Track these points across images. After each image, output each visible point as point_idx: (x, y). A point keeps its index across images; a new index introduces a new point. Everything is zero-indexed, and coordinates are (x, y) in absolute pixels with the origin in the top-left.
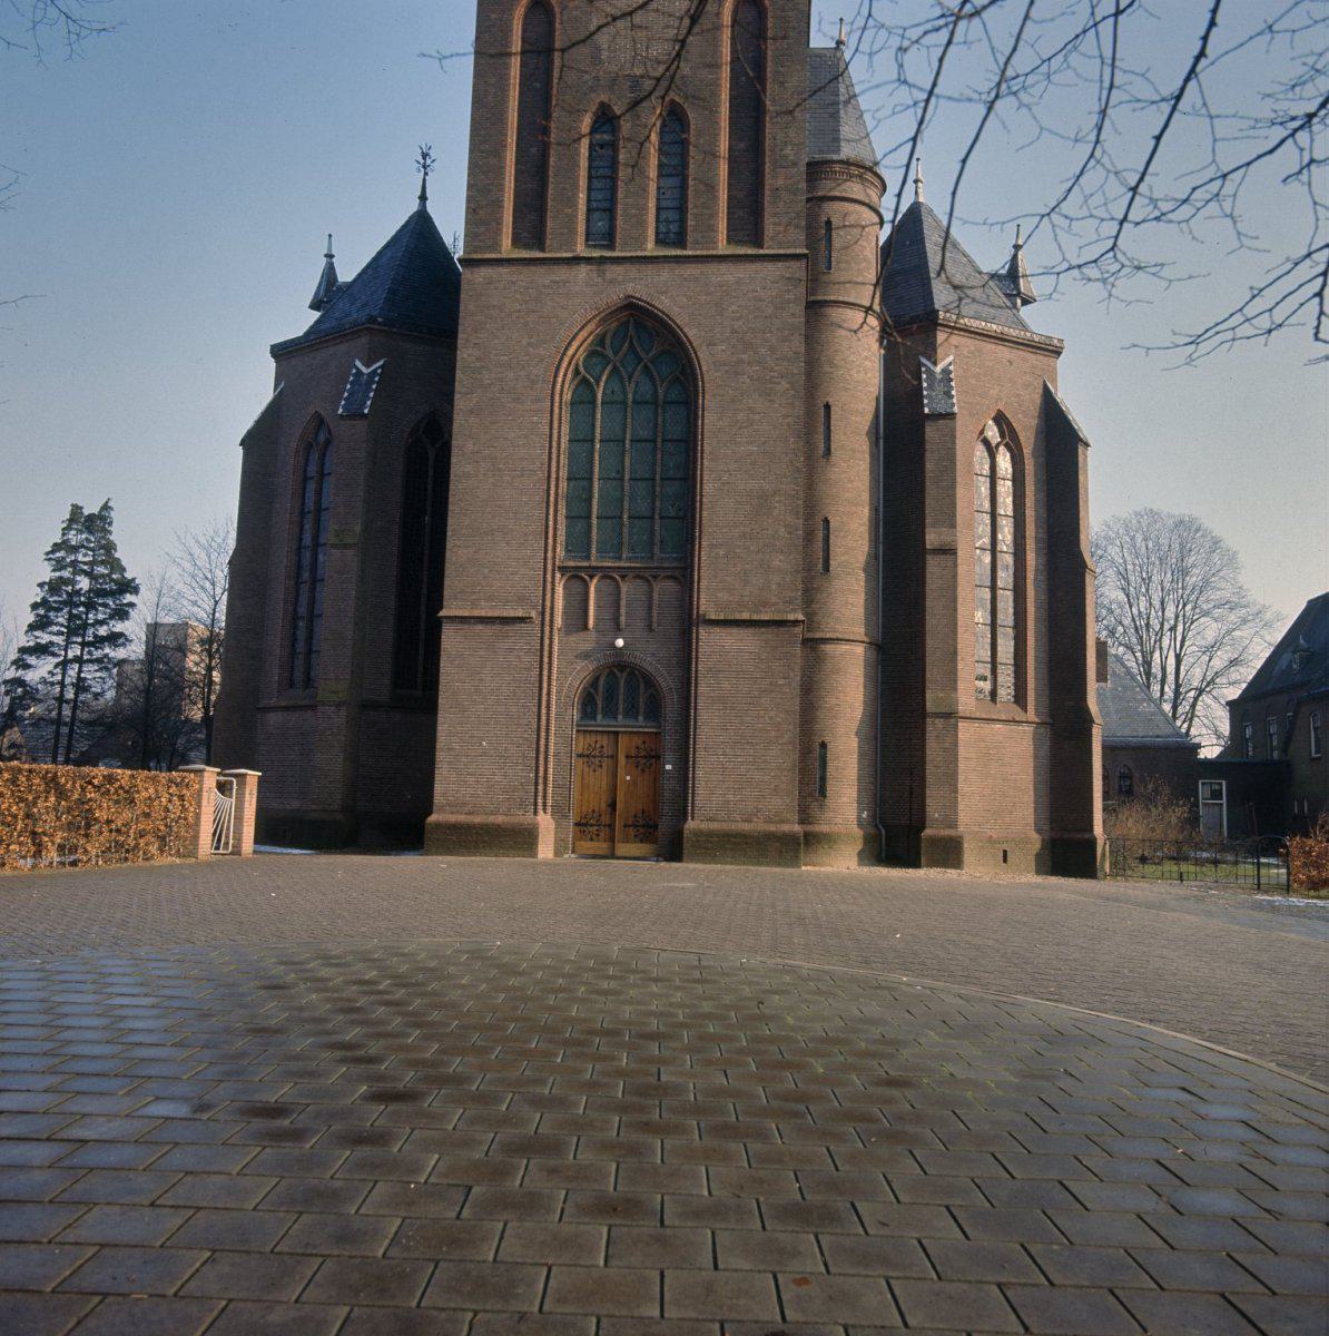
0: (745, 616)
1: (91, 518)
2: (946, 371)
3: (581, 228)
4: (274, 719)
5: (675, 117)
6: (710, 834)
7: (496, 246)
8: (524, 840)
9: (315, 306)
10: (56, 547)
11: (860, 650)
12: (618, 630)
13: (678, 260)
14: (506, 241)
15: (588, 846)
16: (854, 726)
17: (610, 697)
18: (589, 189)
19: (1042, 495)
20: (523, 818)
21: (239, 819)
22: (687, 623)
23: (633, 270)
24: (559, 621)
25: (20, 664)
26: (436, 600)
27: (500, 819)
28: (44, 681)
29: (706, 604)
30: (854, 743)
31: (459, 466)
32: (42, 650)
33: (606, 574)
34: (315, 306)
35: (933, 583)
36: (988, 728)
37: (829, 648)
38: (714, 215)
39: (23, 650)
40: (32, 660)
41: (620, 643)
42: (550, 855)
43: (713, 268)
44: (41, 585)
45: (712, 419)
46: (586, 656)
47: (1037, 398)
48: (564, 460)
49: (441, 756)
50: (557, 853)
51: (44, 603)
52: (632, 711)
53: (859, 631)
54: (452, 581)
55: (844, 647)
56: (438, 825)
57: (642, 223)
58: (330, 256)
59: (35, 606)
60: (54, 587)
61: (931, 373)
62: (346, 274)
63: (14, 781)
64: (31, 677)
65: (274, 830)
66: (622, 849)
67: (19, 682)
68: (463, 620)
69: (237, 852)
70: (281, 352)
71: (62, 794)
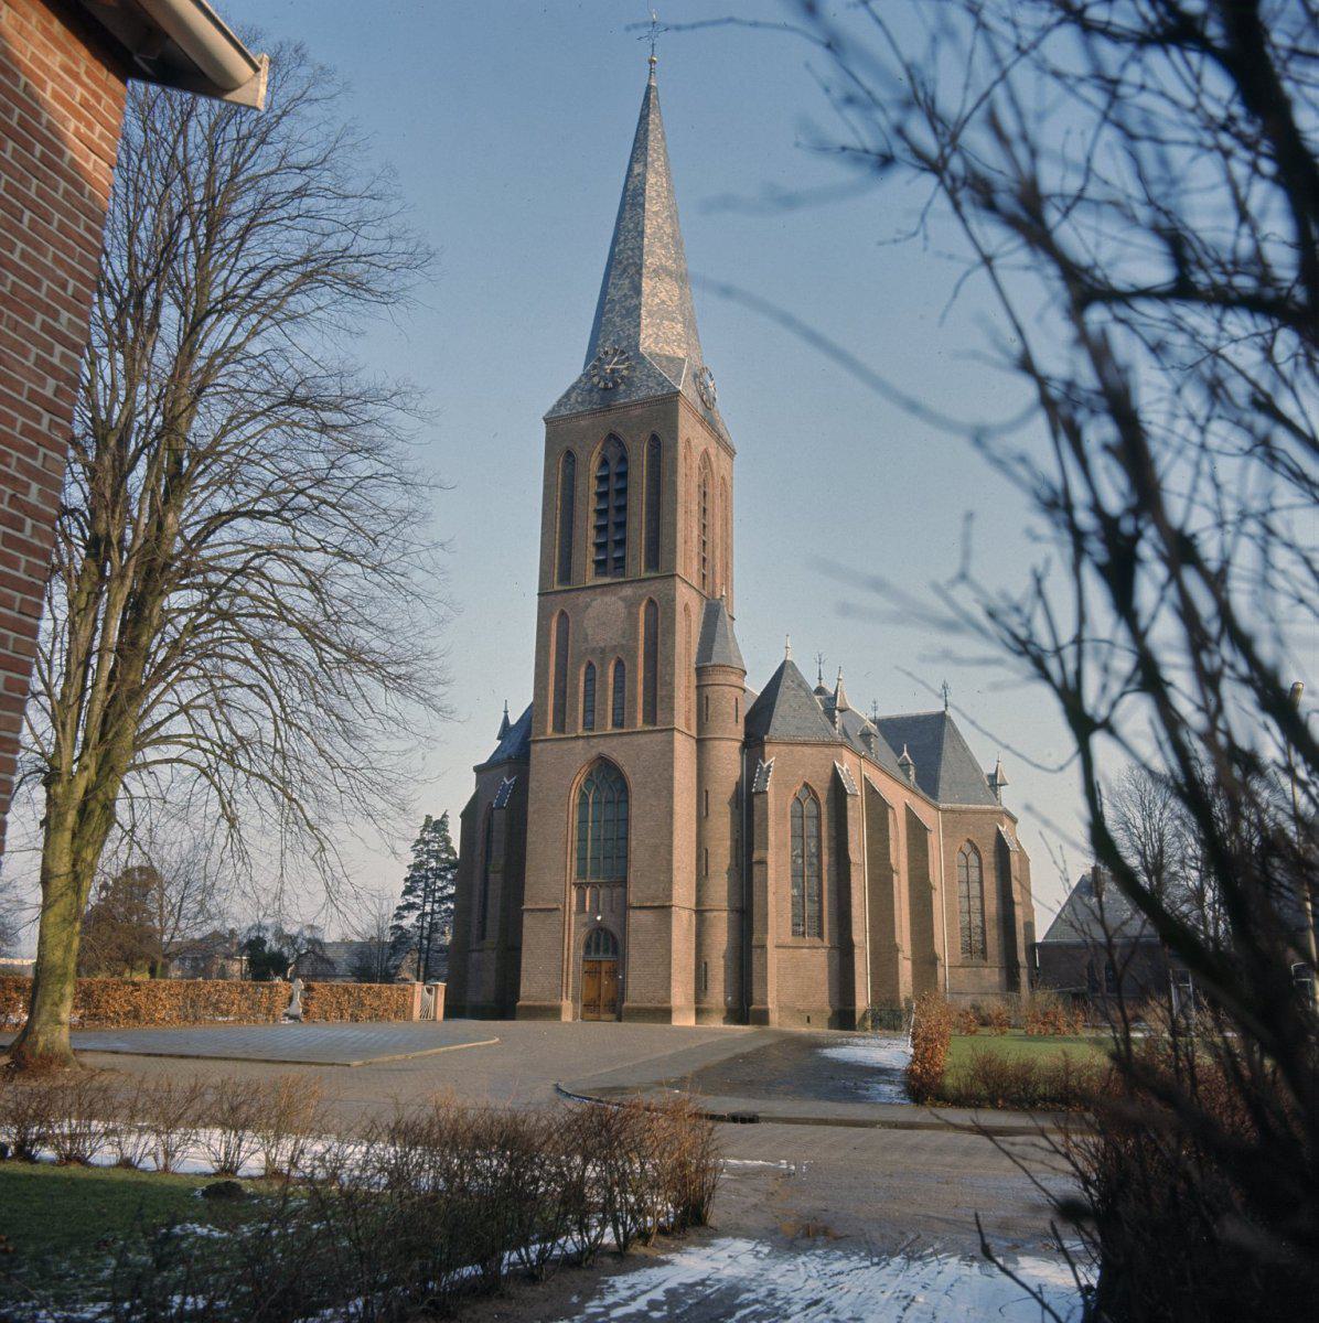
0: (649, 904)
1: (437, 822)
2: (769, 766)
3: (580, 721)
4: (475, 955)
5: (620, 664)
6: (633, 1009)
7: (544, 733)
8: (553, 1012)
9: (499, 738)
10: (418, 842)
11: (725, 914)
12: (598, 913)
13: (621, 734)
14: (550, 730)
15: (591, 1015)
16: (722, 953)
17: (598, 945)
18: (585, 701)
19: (833, 824)
20: (555, 1002)
21: (436, 1005)
22: (626, 907)
23: (602, 741)
24: (574, 908)
25: (399, 916)
26: (521, 901)
27: (546, 1003)
28: (413, 926)
29: (633, 900)
30: (722, 962)
31: (531, 837)
32: (410, 907)
33: (593, 885)
34: (499, 738)
35: (756, 880)
36: (799, 952)
37: (708, 914)
38: (635, 711)
39: (399, 908)
40: (405, 913)
41: (599, 918)
42: (570, 1020)
43: (635, 737)
44: (409, 867)
45: (635, 810)
46: (585, 925)
47: (829, 771)
48: (575, 832)
49: (523, 974)
50: (574, 1019)
51: (412, 876)
52: (606, 951)
53: (725, 904)
54: (527, 893)
55: (715, 913)
56: (521, 1007)
57: (605, 717)
58: (506, 712)
59: (406, 880)
60: (416, 867)
61: (761, 768)
62: (513, 721)
63: (331, 989)
64: (406, 923)
65: (454, 1010)
66: (603, 1017)
67: (399, 927)
68: (532, 910)
69: (434, 1020)
70: (478, 769)
71: (350, 994)
